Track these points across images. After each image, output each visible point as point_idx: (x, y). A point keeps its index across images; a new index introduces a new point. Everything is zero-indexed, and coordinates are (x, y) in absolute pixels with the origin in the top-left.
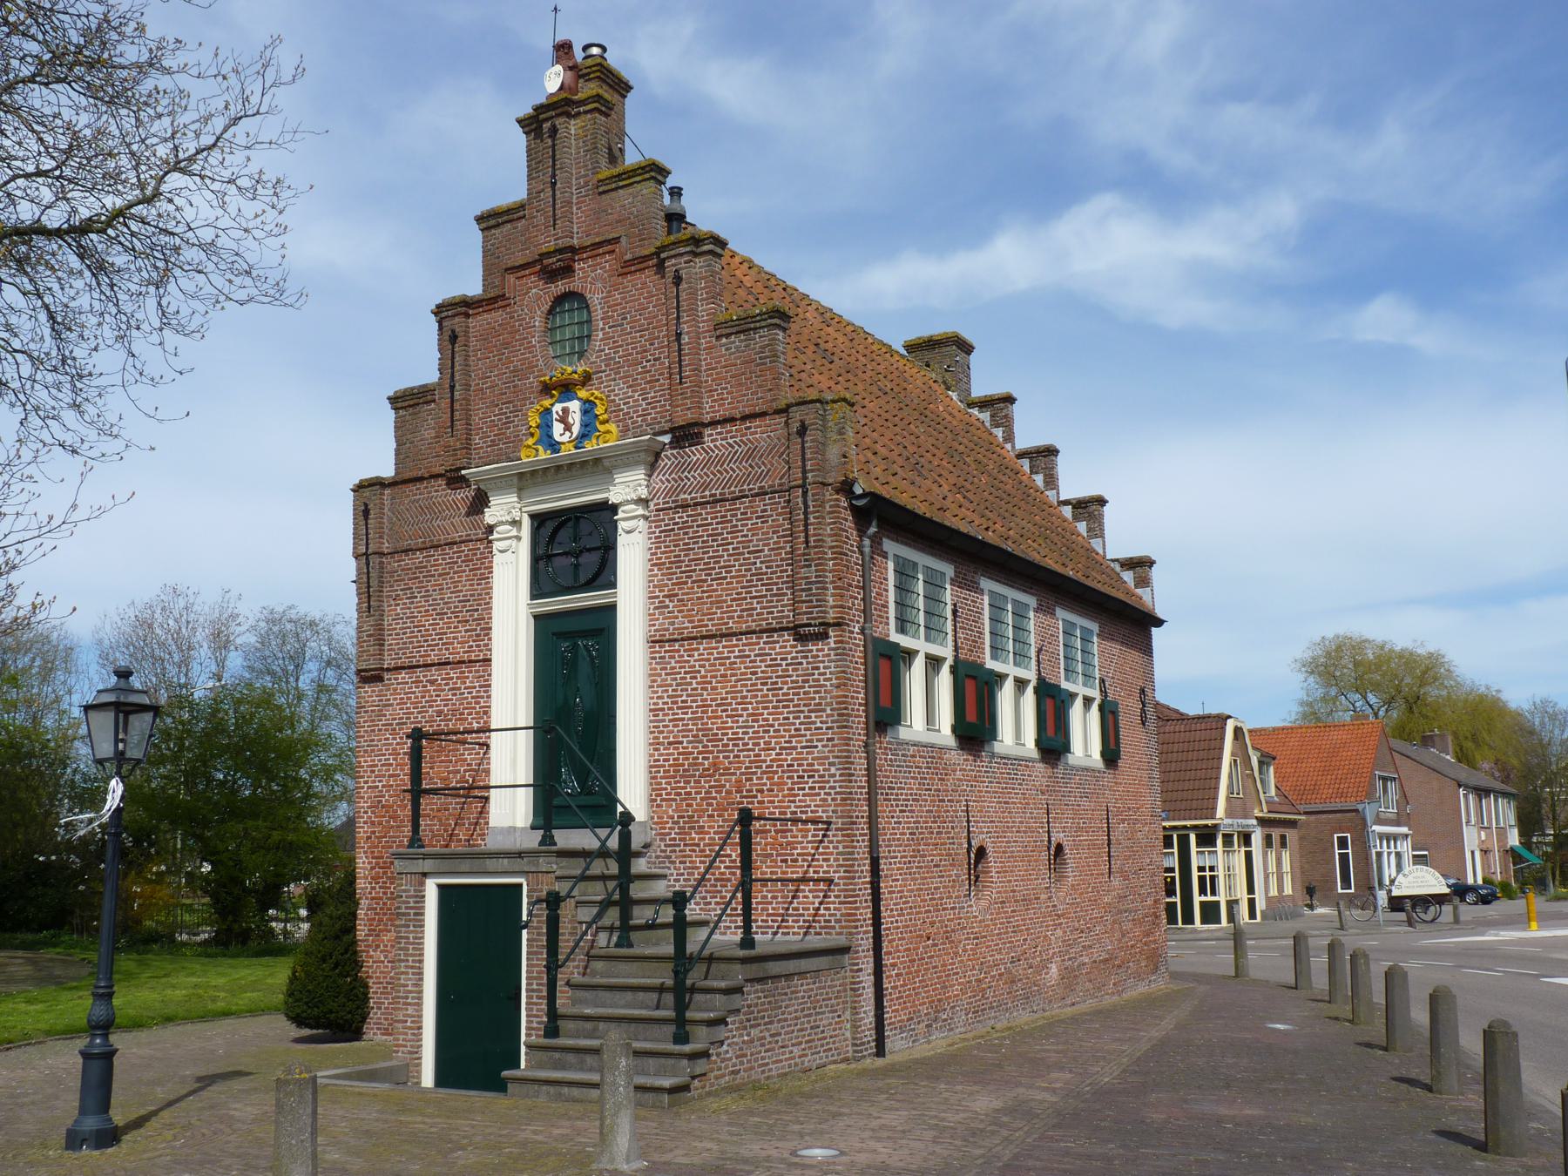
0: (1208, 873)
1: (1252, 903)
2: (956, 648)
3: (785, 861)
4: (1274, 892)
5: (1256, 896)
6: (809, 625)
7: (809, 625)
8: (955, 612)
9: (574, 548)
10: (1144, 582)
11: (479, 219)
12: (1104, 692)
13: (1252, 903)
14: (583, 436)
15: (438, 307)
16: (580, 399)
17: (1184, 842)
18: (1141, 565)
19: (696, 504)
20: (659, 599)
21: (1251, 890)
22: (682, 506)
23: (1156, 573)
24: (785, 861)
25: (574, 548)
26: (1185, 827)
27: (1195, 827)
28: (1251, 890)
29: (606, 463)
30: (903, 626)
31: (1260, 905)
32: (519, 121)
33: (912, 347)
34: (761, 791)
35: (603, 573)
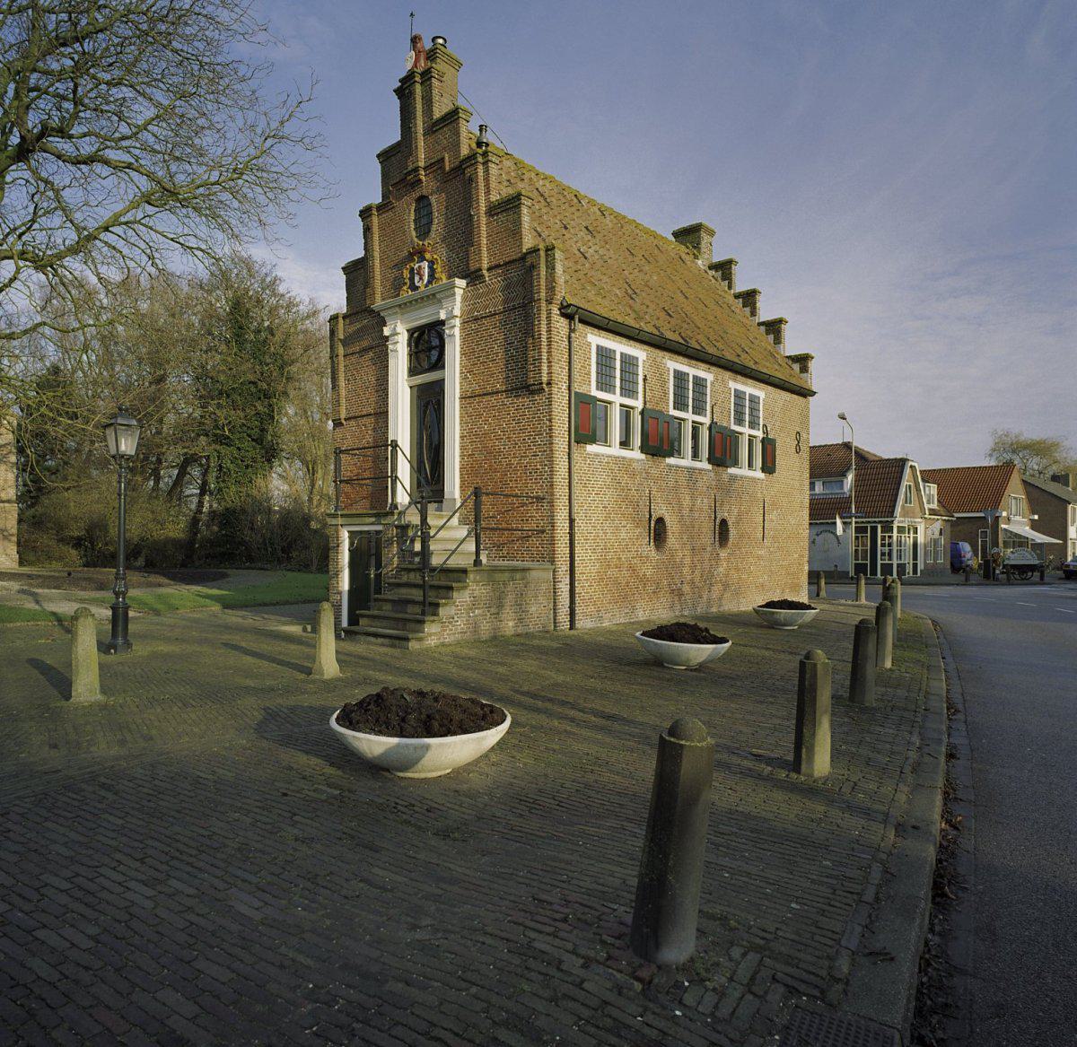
0: (887, 548)
1: (915, 566)
2: (645, 403)
3: (523, 520)
4: (930, 562)
5: (918, 562)
6: (534, 384)
7: (534, 384)
8: (645, 380)
9: (427, 345)
10: (804, 369)
11: (378, 156)
12: (766, 432)
13: (915, 566)
14: (430, 282)
15: (361, 212)
16: (427, 261)
17: (874, 530)
18: (803, 361)
19: (482, 318)
20: (467, 372)
21: (915, 558)
22: (475, 320)
23: (812, 365)
24: (523, 520)
25: (427, 345)
26: (875, 522)
27: (880, 522)
28: (915, 558)
29: (438, 296)
30: (740, 421)
31: (920, 567)
32: (395, 91)
33: (676, 234)
34: (511, 481)
35: (439, 364)
